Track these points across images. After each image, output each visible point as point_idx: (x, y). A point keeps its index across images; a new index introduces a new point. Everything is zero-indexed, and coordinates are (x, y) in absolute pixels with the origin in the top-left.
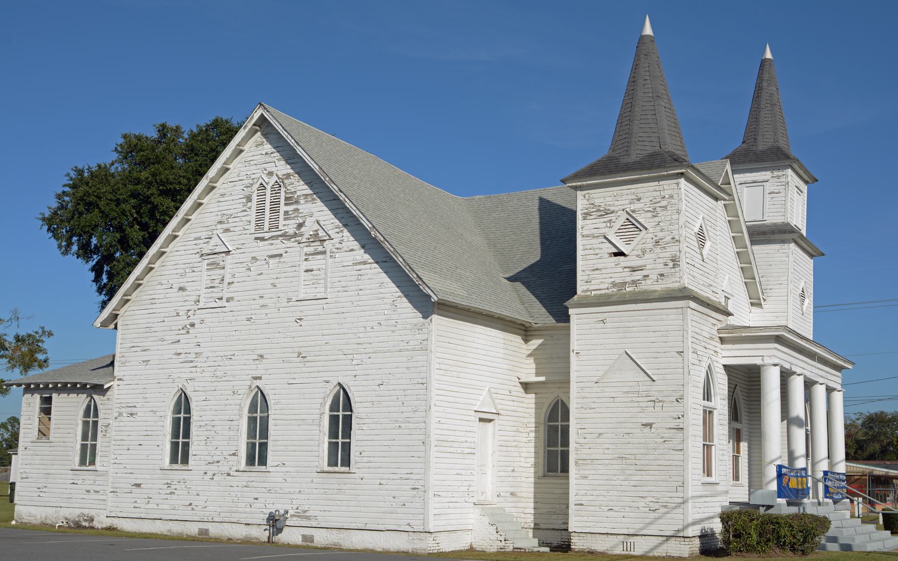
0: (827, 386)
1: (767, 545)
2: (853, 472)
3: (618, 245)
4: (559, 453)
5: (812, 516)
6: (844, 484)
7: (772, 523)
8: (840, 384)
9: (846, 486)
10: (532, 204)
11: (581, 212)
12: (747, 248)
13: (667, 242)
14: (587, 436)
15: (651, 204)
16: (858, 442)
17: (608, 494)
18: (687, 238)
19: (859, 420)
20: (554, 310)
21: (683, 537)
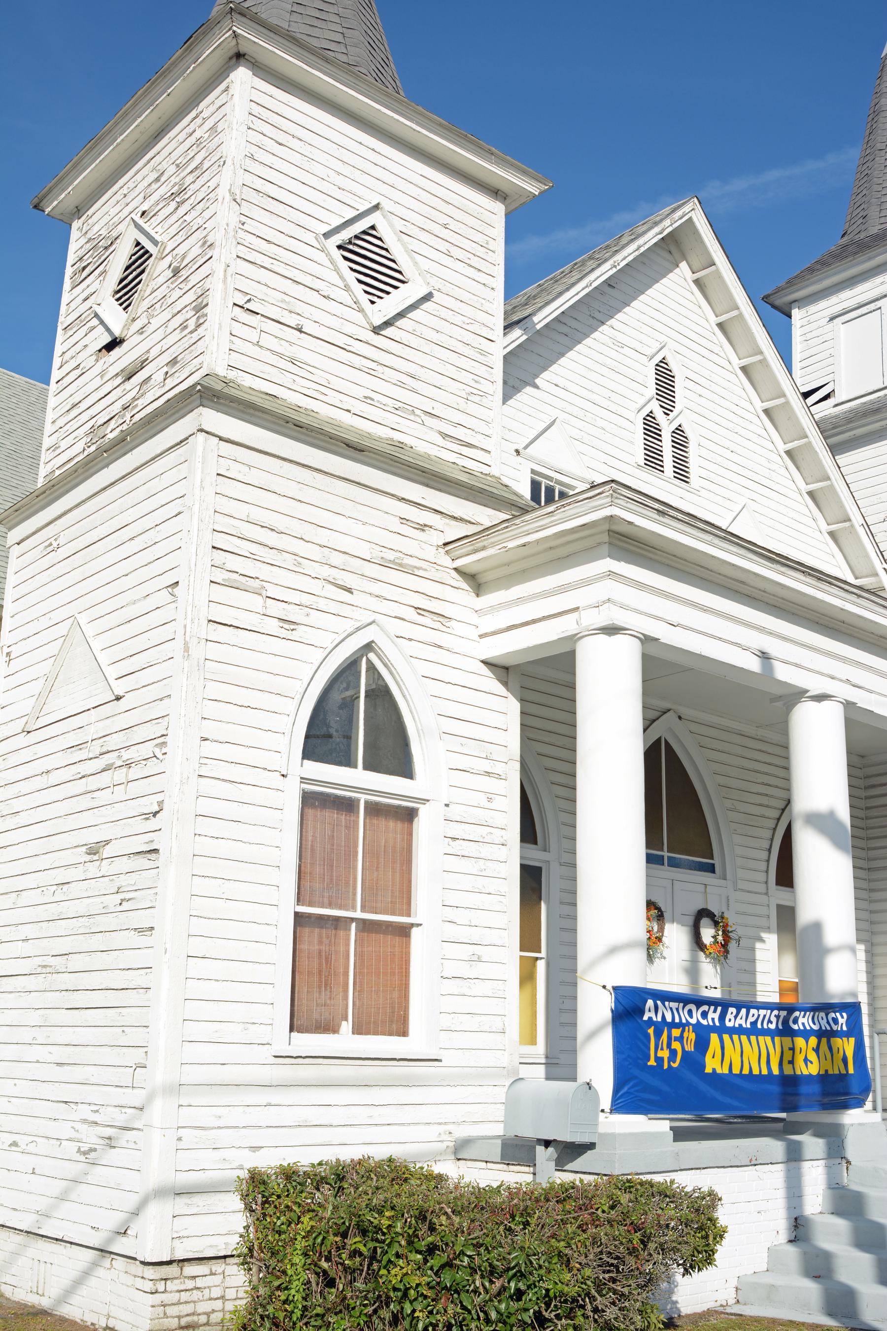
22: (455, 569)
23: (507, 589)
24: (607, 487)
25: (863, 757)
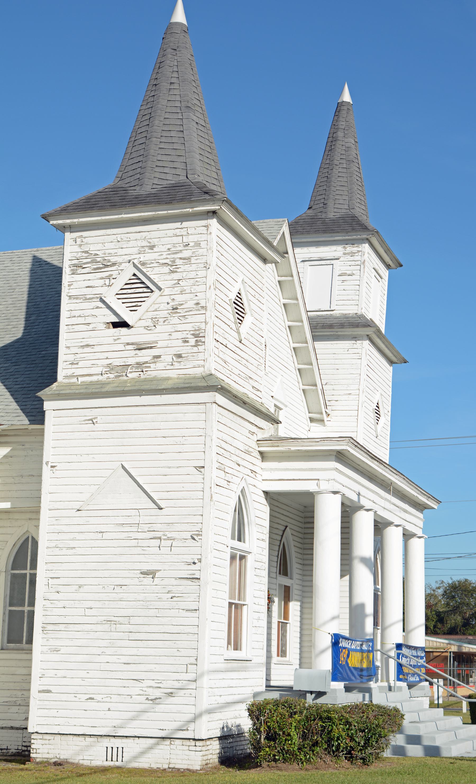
0: (404, 529)
1: (313, 751)
2: (431, 648)
3: (119, 312)
4: (26, 614)
5: (379, 707)
6: (422, 662)
7: (321, 718)
8: (420, 528)
9: (425, 664)
10: (19, 267)
11: (70, 263)
12: (306, 342)
13: (188, 310)
14: (61, 588)
15: (169, 254)
16: (438, 614)
17: (88, 676)
18: (217, 305)
19: (439, 589)
20: (28, 406)
21: (194, 739)
22: (259, 451)
23: (279, 462)
24: (347, 439)
25: (305, 507)
